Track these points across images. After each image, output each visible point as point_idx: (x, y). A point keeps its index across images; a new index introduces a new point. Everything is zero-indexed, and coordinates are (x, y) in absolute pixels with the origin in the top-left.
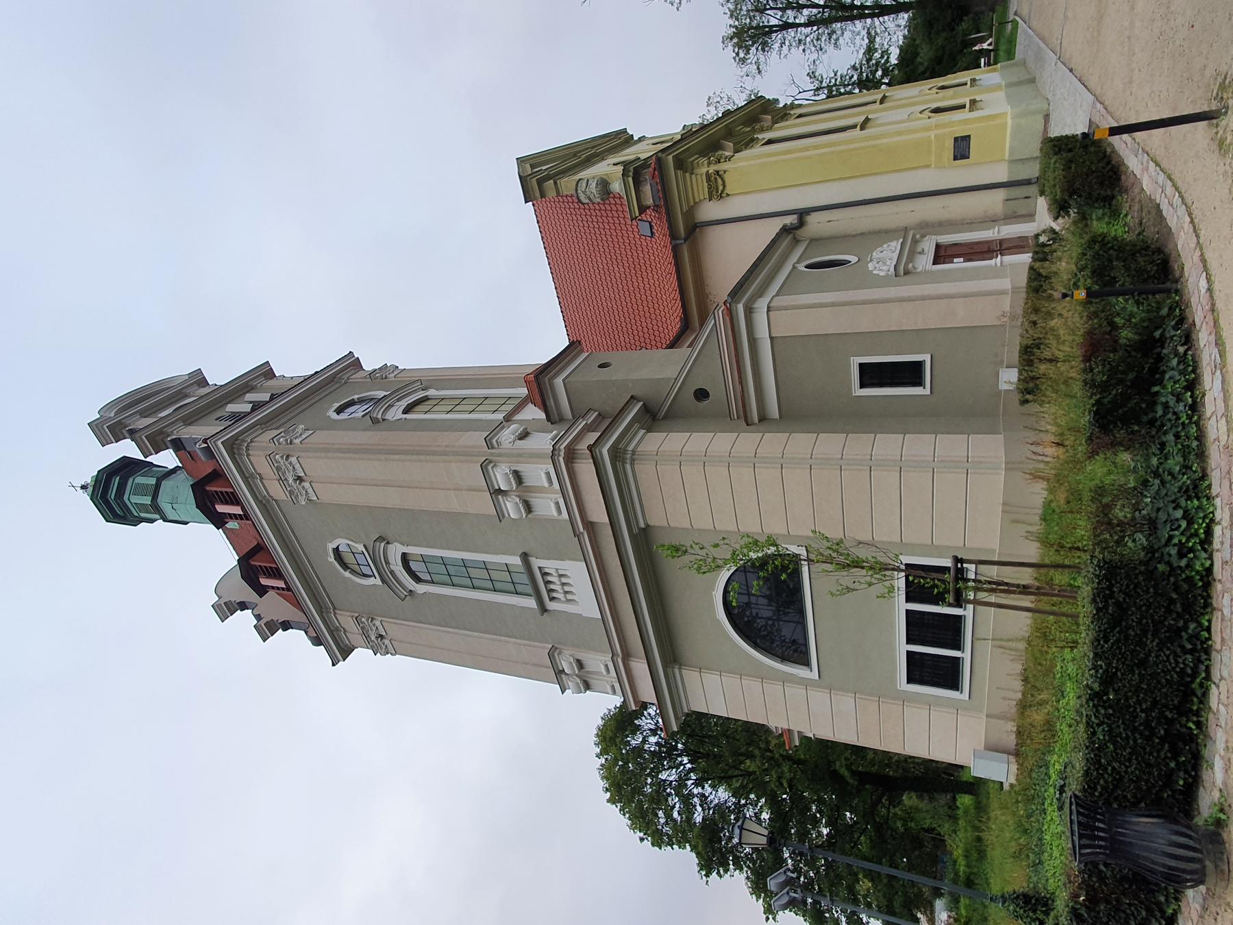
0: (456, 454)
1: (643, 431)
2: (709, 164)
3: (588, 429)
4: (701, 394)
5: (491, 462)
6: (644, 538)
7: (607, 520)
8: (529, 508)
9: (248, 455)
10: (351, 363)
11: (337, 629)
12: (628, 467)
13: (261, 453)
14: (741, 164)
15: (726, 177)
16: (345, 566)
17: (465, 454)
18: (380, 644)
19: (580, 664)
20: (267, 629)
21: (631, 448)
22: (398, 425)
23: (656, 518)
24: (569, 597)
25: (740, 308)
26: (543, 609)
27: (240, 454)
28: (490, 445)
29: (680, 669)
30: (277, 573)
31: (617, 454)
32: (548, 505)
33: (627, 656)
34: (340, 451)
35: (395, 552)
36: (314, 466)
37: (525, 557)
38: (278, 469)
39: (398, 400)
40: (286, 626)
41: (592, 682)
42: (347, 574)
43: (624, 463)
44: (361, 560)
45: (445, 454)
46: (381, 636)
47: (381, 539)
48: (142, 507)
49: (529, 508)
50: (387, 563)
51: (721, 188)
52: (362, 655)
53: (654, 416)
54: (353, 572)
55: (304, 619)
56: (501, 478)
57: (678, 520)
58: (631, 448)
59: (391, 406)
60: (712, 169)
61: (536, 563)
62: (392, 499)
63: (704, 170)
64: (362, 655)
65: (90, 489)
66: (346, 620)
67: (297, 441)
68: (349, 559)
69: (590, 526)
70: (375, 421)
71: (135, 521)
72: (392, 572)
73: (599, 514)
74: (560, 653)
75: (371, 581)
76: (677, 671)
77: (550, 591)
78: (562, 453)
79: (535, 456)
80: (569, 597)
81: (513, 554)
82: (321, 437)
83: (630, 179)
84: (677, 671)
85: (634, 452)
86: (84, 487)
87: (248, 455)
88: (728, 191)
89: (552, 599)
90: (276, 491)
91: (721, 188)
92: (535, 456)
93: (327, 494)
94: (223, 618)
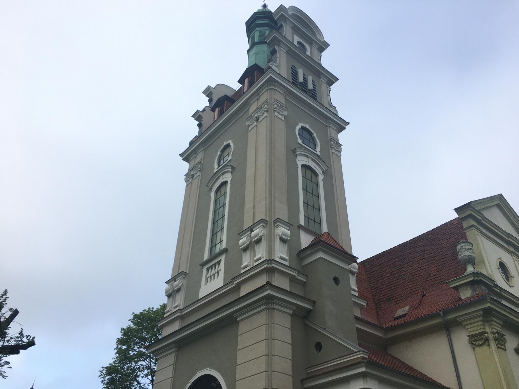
0: (271, 203)
1: (291, 312)
2: (493, 333)
3: (292, 279)
4: (319, 346)
5: (266, 224)
6: (230, 323)
7: (241, 296)
8: (245, 250)
9: (267, 90)
10: (341, 125)
11: (196, 153)
12: (264, 307)
13: (268, 97)
14: (496, 357)
15: (485, 348)
16: (223, 151)
17: (270, 209)
18: (189, 177)
19: (178, 290)
20: (198, 116)
21: (276, 307)
22: (291, 166)
23: (243, 327)
24: (209, 279)
25: (363, 369)
26: (203, 264)
27: (267, 86)
28: (275, 221)
29: (175, 351)
30: (221, 113)
31: (269, 299)
32: (247, 260)
33: (182, 318)
34: (271, 138)
35: (228, 177)
36: (263, 127)
37: (225, 251)
38: (261, 108)
39: (313, 160)
40: (200, 125)
41: (171, 298)
42: (219, 153)
43: (266, 304)
44: (225, 159)
45: (270, 196)
46: (193, 177)
47: (233, 168)
48: (253, 38)
49: (245, 250)
50: (223, 174)
51: (477, 343)
52: (185, 166)
53: (304, 319)
54: (220, 156)
55: (203, 131)
56: (258, 231)
57: (242, 341)
58: (276, 307)
59: (307, 157)
60: (491, 336)
61: (223, 258)
62: (250, 172)
63: (488, 330)
64: (185, 166)
65: (264, 10)
66: (200, 157)
67: (276, 114)
68: (226, 152)
69: (238, 287)
70: (294, 151)
71: (248, 35)
72: (219, 177)
73: (245, 290)
74: (184, 278)
75: (216, 166)
76: (174, 350)
77: (211, 267)
78: (270, 266)
79: (270, 250)
80: (209, 279)
81: (227, 243)
82: (280, 127)
83: (472, 279)
84: (174, 350)
85: (274, 309)
86: (265, 6)
87: (267, 90)
88: (477, 349)
89: (208, 269)
90: (253, 107)
91: (477, 343)
92: (270, 250)
93: (251, 136)
94: (204, 92)
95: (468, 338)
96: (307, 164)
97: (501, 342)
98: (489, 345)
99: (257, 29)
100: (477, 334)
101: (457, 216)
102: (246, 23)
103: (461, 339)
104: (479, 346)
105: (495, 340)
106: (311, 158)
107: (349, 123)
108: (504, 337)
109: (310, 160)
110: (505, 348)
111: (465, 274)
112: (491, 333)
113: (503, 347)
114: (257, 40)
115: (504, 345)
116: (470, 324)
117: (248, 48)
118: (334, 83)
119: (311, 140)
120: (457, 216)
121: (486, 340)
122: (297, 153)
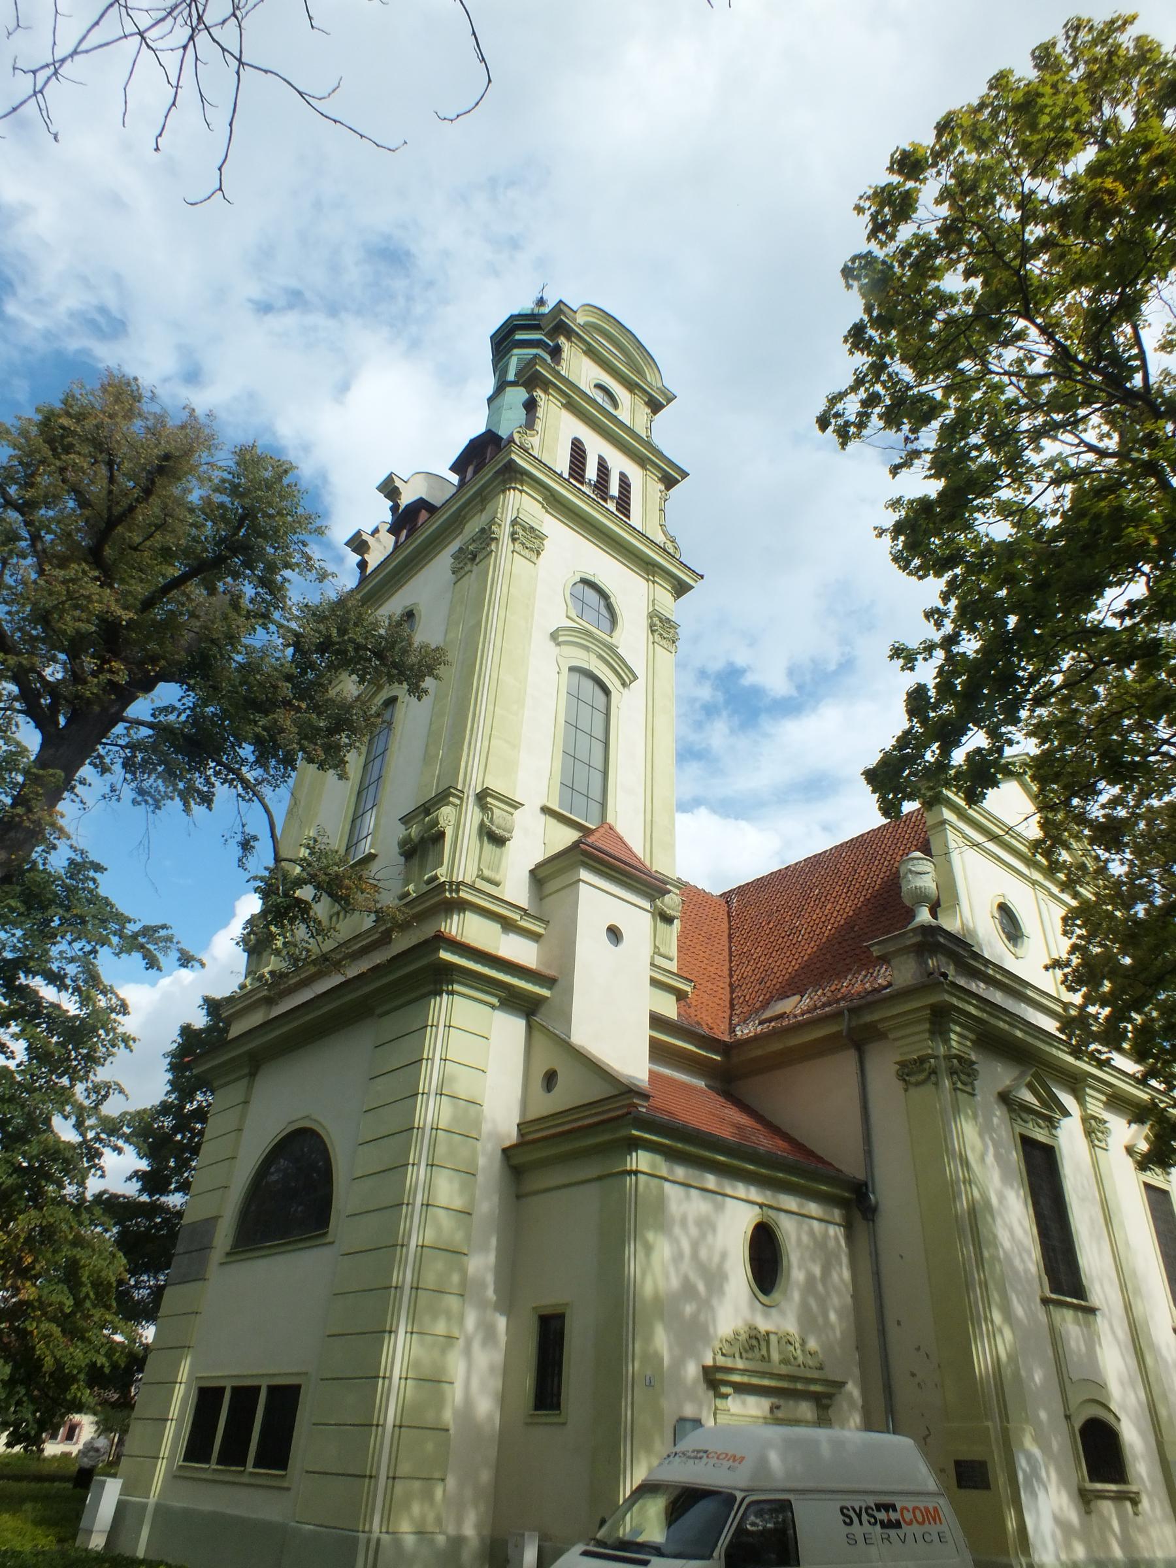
15: (929, 1088)
39: (600, 657)
59: (587, 649)
91: (913, 1079)
95: (898, 1067)
96: (586, 666)
97: (963, 1077)
98: (936, 1084)
99: (516, 351)
100: (915, 1060)
101: (121, 1481)
102: (492, 338)
103: (883, 1067)
104: (918, 1084)
105: (952, 1074)
106: (595, 652)
107: (702, 577)
108: (975, 1067)
109: (593, 657)
110: (974, 1089)
111: (910, 927)
112: (945, 1057)
113: (968, 1089)
114: (511, 376)
115: (972, 1084)
116: (903, 1037)
117: (490, 391)
118: (678, 481)
119: (604, 611)
120: (121, 1481)
121: (930, 1074)
122: (561, 639)
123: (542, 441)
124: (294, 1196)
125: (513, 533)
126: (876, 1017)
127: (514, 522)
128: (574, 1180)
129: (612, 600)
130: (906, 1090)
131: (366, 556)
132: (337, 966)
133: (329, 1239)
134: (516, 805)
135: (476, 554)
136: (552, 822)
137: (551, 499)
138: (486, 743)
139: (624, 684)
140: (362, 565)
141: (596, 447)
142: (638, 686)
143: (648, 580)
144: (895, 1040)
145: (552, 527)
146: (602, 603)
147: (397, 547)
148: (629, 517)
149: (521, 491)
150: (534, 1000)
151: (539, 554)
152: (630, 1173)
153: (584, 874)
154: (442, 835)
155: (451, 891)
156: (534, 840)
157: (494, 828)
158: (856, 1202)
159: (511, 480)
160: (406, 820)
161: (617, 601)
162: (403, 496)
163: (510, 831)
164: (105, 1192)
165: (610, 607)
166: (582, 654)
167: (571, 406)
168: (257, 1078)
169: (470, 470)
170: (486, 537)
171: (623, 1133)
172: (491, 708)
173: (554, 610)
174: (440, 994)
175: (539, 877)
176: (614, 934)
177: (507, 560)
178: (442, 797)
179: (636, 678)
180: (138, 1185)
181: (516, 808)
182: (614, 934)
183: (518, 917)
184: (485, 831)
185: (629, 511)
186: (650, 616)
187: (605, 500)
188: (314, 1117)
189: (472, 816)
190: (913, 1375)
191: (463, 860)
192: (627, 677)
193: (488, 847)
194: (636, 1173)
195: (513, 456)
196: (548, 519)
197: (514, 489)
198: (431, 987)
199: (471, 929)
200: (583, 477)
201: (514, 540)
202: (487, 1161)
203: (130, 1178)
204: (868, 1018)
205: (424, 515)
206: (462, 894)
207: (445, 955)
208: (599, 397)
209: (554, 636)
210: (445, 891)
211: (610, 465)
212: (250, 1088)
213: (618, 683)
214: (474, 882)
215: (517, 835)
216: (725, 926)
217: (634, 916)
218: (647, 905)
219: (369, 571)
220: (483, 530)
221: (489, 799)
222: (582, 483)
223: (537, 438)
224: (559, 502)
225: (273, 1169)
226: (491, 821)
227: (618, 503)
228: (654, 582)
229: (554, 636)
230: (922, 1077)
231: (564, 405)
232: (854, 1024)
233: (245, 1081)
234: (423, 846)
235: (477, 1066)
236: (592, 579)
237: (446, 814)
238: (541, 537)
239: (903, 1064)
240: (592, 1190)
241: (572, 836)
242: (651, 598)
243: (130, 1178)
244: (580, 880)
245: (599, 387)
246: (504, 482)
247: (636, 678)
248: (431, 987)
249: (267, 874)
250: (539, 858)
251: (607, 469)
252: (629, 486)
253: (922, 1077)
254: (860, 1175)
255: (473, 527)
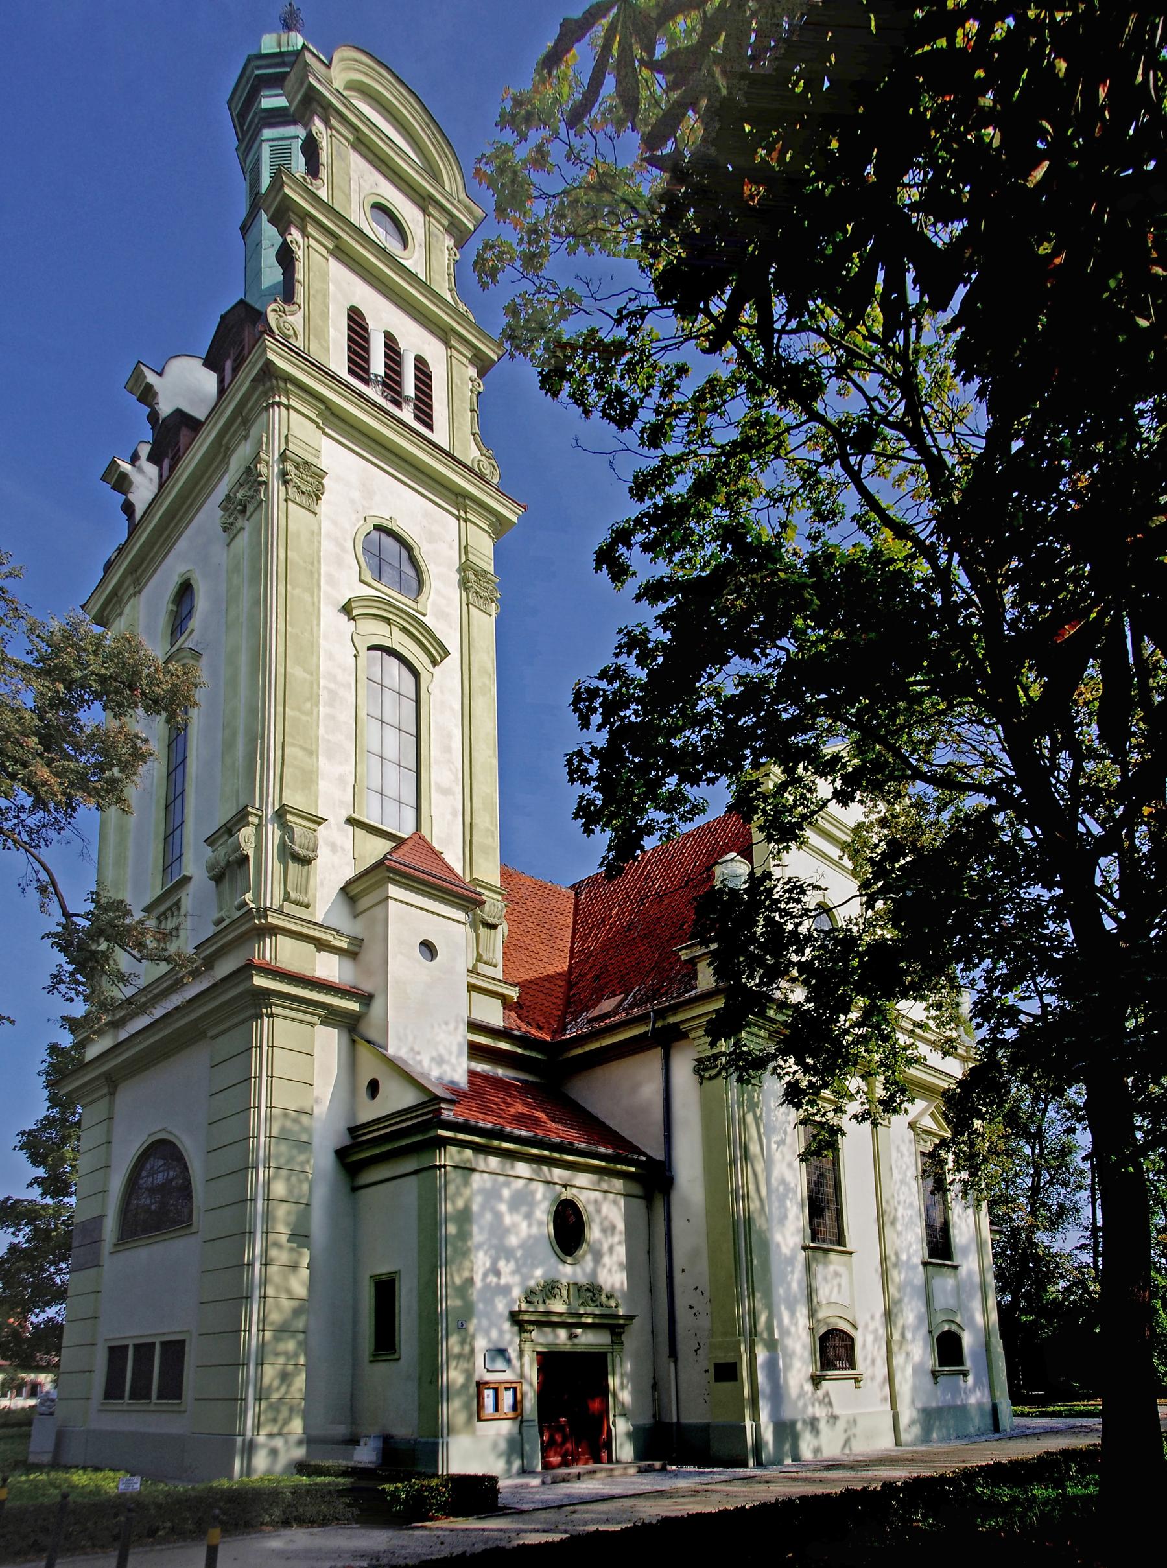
39: (404, 630)
59: (388, 621)
91: (707, 1075)
104: (710, 1078)
106: (397, 625)
109: (395, 630)
122: (355, 613)
123: (307, 319)
124: (161, 1197)
125: (284, 474)
126: (678, 1018)
127: (283, 457)
128: (397, 1174)
129: (416, 551)
130: (701, 1084)
131: (132, 497)
132: (142, 1009)
133: (193, 1229)
134: (319, 821)
135: (247, 502)
136: (360, 833)
137: (328, 413)
138: (279, 753)
139: (435, 663)
140: (128, 508)
141: (383, 317)
142: (452, 663)
143: (458, 518)
144: (695, 1039)
145: (335, 458)
146: (404, 554)
147: (222, 390)
148: (430, 427)
149: (288, 407)
150: (355, 1020)
151: (318, 498)
152: (440, 1167)
153: (394, 891)
154: (247, 856)
155: (259, 918)
156: (337, 859)
157: (296, 848)
158: (652, 1181)
159: (273, 391)
160: (211, 841)
161: (423, 551)
162: (161, 399)
163: (314, 850)
164: (9, 1198)
165: (413, 561)
166: (382, 628)
167: (341, 253)
168: (117, 1095)
169: (228, 365)
170: (251, 478)
171: (431, 1134)
172: (280, 709)
173: (343, 577)
174: (261, 1017)
175: (350, 893)
176: (429, 949)
177: (285, 512)
178: (241, 818)
179: (447, 654)
180: (40, 1191)
181: (319, 824)
182: (429, 949)
183: (330, 938)
184: (288, 852)
185: (431, 417)
186: (463, 568)
187: (398, 404)
188: (169, 1129)
189: (273, 834)
190: (691, 1307)
191: (272, 887)
192: (438, 654)
193: (293, 867)
194: (445, 1166)
195: (271, 356)
196: (326, 444)
197: (279, 404)
198: (252, 1011)
199: (287, 953)
200: (367, 371)
201: (286, 483)
202: (321, 1160)
203: (30, 1185)
204: (672, 1020)
205: (184, 434)
206: (270, 920)
207: (259, 981)
208: (380, 233)
209: (346, 609)
210: (253, 918)
211: (402, 346)
212: (111, 1104)
213: (427, 661)
214: (282, 906)
215: (323, 853)
216: (570, 920)
217: (449, 928)
218: (460, 915)
219: (138, 514)
220: (248, 471)
221: (289, 817)
222: (366, 382)
223: (300, 314)
224: (338, 417)
225: (144, 1174)
226: (292, 841)
227: (416, 407)
228: (466, 520)
229: (346, 609)
230: (715, 1071)
231: (331, 253)
232: (659, 1024)
233: (106, 1100)
234: (231, 870)
235: (303, 1078)
236: (388, 524)
237: (246, 834)
238: (320, 475)
239: (699, 1061)
240: (412, 1181)
241: (384, 846)
242: (463, 544)
243: (30, 1185)
244: (388, 898)
245: (382, 209)
246: (266, 394)
247: (447, 654)
248: (252, 1011)
249: (59, 929)
250: (349, 874)
251: (398, 353)
252: (430, 377)
253: (715, 1071)
254: (658, 1155)
255: (241, 455)
